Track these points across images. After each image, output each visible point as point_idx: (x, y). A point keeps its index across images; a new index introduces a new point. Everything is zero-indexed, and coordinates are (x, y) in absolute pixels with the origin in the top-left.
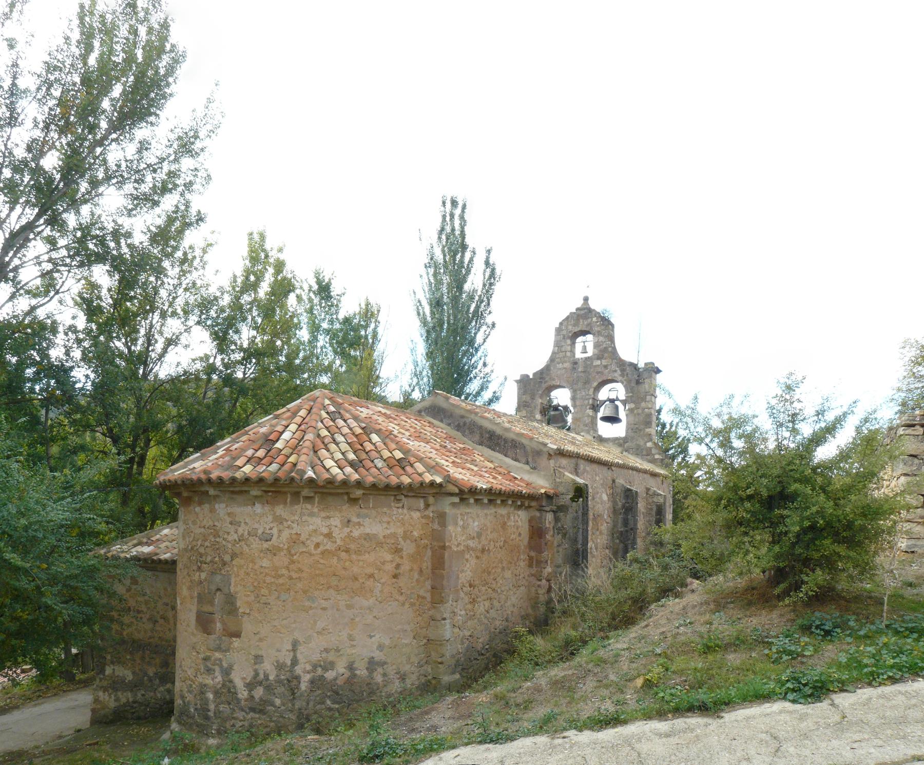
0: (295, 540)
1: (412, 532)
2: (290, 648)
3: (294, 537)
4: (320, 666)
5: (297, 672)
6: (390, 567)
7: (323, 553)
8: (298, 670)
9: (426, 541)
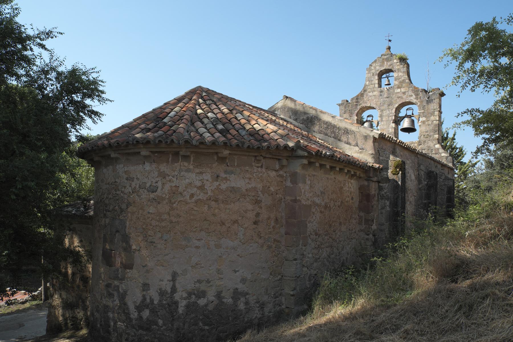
0: (175, 191)
1: (269, 187)
2: (170, 278)
3: (174, 188)
4: (194, 294)
5: (176, 298)
6: (251, 215)
7: (196, 202)
8: (177, 297)
9: (281, 196)
